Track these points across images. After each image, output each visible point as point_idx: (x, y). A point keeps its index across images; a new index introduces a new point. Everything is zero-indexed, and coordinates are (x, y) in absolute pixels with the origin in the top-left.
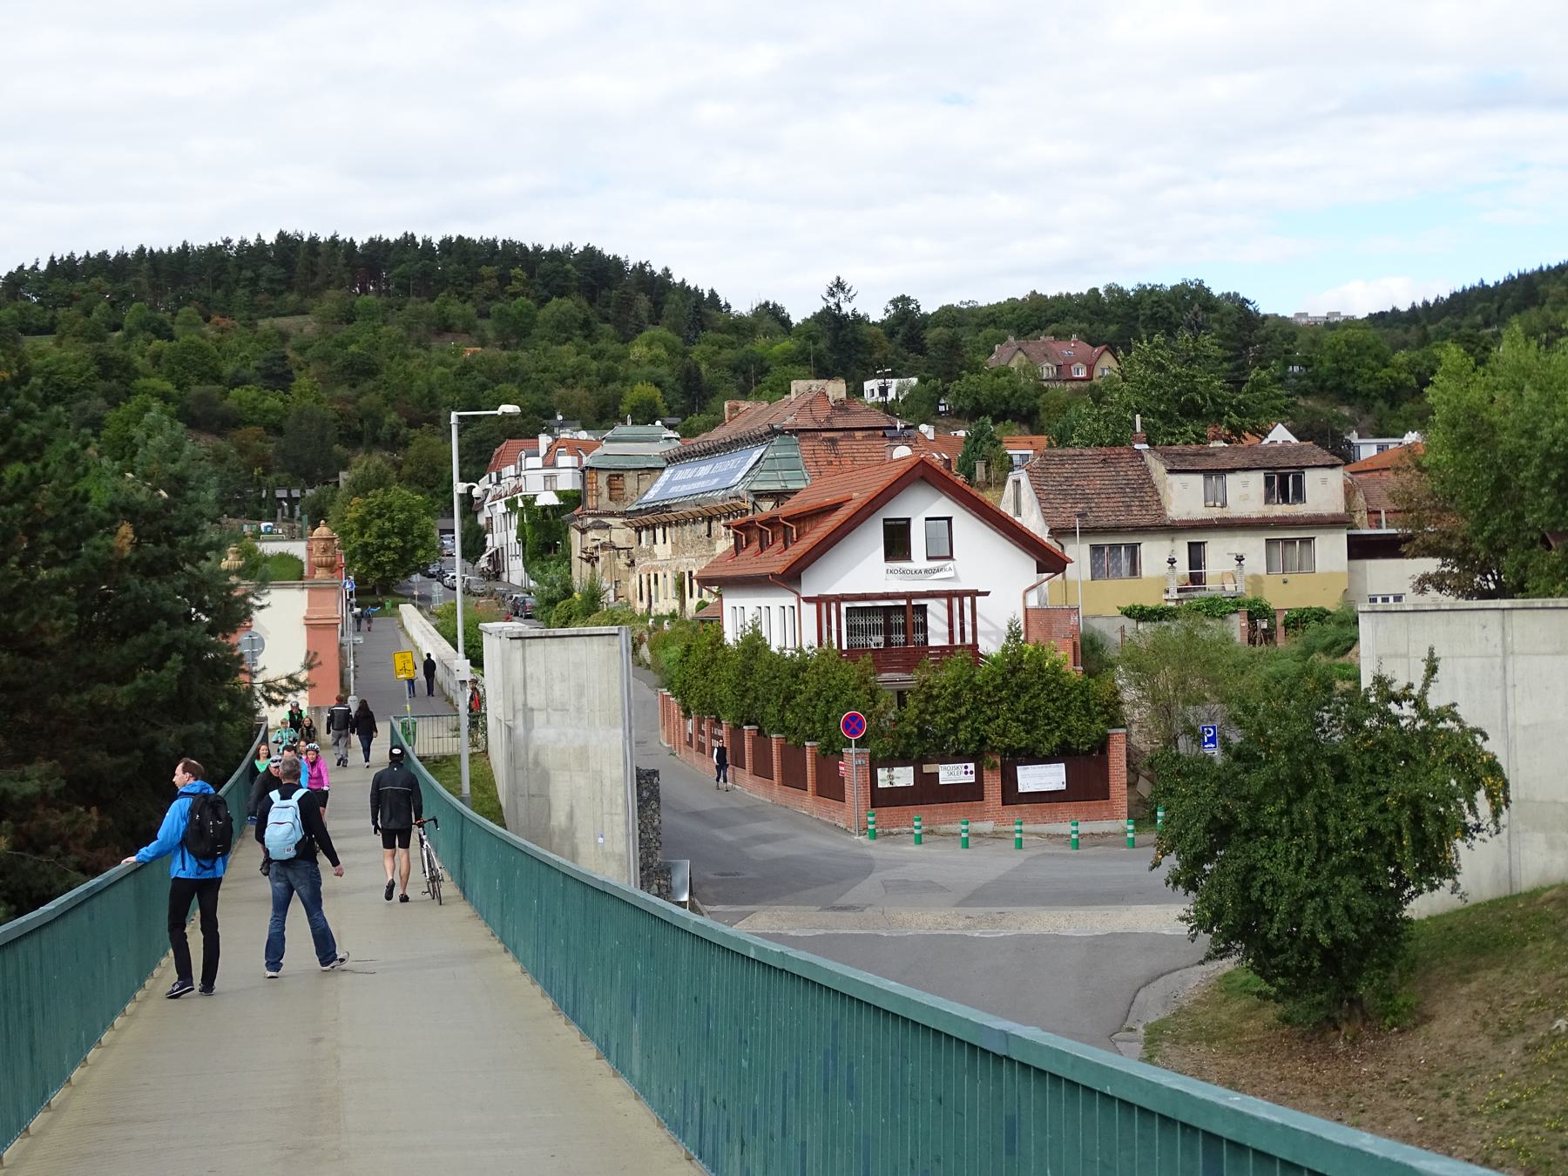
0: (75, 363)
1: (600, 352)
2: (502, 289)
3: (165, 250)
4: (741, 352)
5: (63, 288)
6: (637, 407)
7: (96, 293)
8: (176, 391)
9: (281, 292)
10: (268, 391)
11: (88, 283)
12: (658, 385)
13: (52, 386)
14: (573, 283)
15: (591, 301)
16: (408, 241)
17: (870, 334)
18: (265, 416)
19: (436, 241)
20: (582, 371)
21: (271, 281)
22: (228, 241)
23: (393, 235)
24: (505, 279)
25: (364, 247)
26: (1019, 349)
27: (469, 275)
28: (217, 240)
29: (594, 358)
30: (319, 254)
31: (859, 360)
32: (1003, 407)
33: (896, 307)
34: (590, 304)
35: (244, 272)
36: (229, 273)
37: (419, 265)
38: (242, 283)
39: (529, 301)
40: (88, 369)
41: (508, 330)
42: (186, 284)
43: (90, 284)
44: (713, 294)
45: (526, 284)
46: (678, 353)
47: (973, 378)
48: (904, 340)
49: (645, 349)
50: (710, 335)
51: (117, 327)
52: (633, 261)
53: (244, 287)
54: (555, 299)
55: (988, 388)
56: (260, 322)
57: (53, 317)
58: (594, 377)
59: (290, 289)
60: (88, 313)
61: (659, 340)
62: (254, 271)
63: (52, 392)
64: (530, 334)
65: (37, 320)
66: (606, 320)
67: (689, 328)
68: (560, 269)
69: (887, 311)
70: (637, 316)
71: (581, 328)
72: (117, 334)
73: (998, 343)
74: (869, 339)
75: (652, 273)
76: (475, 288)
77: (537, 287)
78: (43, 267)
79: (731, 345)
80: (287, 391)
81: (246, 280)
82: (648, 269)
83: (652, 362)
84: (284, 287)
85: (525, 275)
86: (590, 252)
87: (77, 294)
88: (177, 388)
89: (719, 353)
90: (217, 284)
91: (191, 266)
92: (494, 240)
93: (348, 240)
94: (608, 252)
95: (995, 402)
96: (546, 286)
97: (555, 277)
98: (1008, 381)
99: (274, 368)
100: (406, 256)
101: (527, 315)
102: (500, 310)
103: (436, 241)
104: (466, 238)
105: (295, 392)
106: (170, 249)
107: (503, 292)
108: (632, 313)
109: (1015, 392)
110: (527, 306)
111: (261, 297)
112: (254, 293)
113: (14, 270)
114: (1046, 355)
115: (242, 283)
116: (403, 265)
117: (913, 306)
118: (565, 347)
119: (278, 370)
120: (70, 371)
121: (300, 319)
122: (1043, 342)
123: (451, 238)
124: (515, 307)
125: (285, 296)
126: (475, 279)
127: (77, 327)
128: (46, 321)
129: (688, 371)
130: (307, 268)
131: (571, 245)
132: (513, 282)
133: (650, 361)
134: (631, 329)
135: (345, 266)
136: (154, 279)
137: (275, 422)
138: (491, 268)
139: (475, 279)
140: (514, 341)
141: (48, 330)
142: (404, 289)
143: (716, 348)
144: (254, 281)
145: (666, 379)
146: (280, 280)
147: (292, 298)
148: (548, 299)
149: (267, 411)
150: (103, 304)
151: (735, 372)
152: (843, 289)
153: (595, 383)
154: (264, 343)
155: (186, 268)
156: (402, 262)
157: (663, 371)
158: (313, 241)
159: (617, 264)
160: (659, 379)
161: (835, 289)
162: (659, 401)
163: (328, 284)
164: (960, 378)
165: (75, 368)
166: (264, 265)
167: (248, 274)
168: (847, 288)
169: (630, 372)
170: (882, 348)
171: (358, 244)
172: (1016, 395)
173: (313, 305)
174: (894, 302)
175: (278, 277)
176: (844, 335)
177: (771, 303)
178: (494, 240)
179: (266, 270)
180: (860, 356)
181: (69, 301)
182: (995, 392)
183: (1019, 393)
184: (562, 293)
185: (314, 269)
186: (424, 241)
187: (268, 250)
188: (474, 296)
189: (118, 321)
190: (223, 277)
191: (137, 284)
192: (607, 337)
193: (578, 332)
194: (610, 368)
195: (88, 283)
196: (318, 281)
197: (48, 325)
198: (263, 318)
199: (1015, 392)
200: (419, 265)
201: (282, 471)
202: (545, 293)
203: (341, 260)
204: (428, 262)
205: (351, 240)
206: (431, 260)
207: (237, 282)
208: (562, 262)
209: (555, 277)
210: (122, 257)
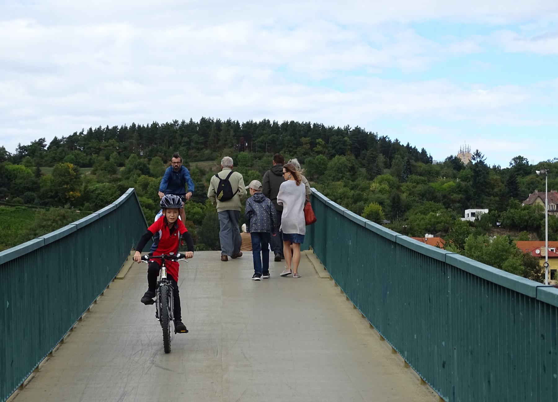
0: (110, 189)
1: (355, 186)
2: (312, 150)
3: (146, 126)
4: (426, 187)
5: (95, 145)
6: (370, 214)
7: (111, 147)
8: (154, 203)
9: (202, 149)
10: (195, 203)
11: (108, 142)
12: (381, 203)
13: (99, 200)
14: (348, 147)
15: (357, 156)
16: (265, 123)
17: (493, 179)
18: (193, 216)
19: (280, 123)
20: (345, 196)
21: (197, 143)
22: (176, 122)
23: (257, 120)
24: (313, 144)
25: (243, 125)
26: (539, 197)
27: (295, 142)
28: (170, 121)
29: (352, 189)
30: (221, 130)
31: (487, 192)
32: (525, 224)
33: (516, 162)
34: (356, 157)
35: (184, 138)
36: (177, 139)
37: (271, 136)
38: (183, 144)
39: (324, 157)
40: (115, 192)
41: (313, 171)
42: (156, 144)
43: (109, 143)
44: (424, 151)
45: (323, 147)
46: (395, 187)
47: (512, 211)
48: (508, 184)
49: (378, 185)
50: (414, 177)
51: (121, 165)
52: (380, 135)
53: (184, 146)
54: (337, 156)
55: (518, 215)
56: (191, 164)
57: (91, 159)
58: (350, 199)
59: (206, 147)
60: (108, 159)
61: (386, 180)
62: (188, 138)
63: (99, 203)
64: (324, 174)
65: (83, 160)
66: (363, 166)
67: (404, 172)
68: (341, 139)
69: (511, 164)
70: (377, 166)
71: (350, 171)
72: (122, 169)
73: (530, 193)
74: (492, 182)
75: (390, 141)
76: (298, 149)
77: (329, 148)
78: (85, 133)
79: (424, 182)
80: (204, 203)
81: (185, 142)
82: (387, 140)
83: (380, 191)
84: (203, 146)
85: (323, 143)
86: (358, 130)
87: (102, 148)
88: (154, 202)
89: (416, 187)
90: (170, 144)
91: (158, 135)
92: (309, 123)
93: (236, 122)
94: (367, 130)
95: (521, 222)
96: (334, 148)
97: (339, 144)
98: (528, 212)
99: (198, 192)
100: (265, 132)
101: (323, 164)
102: (309, 161)
103: (280, 123)
104: (295, 122)
105: (208, 204)
106: (148, 126)
107: (313, 151)
108: (375, 165)
109: (531, 217)
110: (323, 159)
111: (191, 151)
112: (188, 149)
113: (72, 134)
114: (552, 200)
115: (183, 144)
116: (263, 136)
117: (525, 161)
118: (339, 183)
119: (200, 193)
120: (107, 194)
121: (210, 163)
122: (552, 193)
123: (287, 122)
124: (317, 160)
125: (204, 151)
126: (299, 144)
127: (103, 165)
128: (87, 161)
129: (394, 199)
130: (215, 137)
131: (349, 126)
132: (318, 146)
133: (380, 191)
134: (374, 172)
135: (234, 136)
136: (140, 141)
137: (198, 219)
138: (307, 139)
139: (299, 144)
140: (315, 176)
141: (89, 165)
142: (263, 149)
143: (414, 184)
144: (188, 143)
145: (386, 200)
146: (201, 143)
147: (207, 152)
148: (334, 156)
149: (195, 214)
150: (115, 153)
151: (423, 197)
152: (480, 156)
153: (351, 202)
154: (193, 177)
155: (156, 136)
156: (262, 135)
157: (384, 197)
158: (218, 122)
159: (372, 137)
160: (382, 201)
161: (475, 156)
162: (380, 212)
163: (225, 145)
164: (506, 210)
165: (110, 192)
166: (194, 135)
167: (186, 139)
168: (482, 155)
169: (369, 196)
170: (499, 186)
171: (241, 124)
172: (531, 219)
173: (218, 156)
174: (514, 159)
175: (200, 141)
176: (479, 179)
177: (454, 156)
178: (309, 123)
179: (195, 137)
180: (487, 190)
181: (98, 151)
182: (522, 217)
183: (532, 218)
184: (342, 152)
185: (219, 137)
186: (274, 123)
187: (196, 126)
188: (298, 153)
189: (122, 161)
190: (174, 141)
191: (131, 143)
192: (362, 176)
193: (348, 173)
194: (359, 194)
195: (108, 142)
196: (220, 143)
197: (88, 163)
198: (192, 162)
199: (531, 217)
200: (271, 136)
201: (201, 243)
202: (334, 151)
203: (232, 133)
204: (275, 135)
205: (238, 122)
206: (277, 134)
207: (180, 143)
208: (342, 135)
209: (339, 144)
210: (124, 129)
